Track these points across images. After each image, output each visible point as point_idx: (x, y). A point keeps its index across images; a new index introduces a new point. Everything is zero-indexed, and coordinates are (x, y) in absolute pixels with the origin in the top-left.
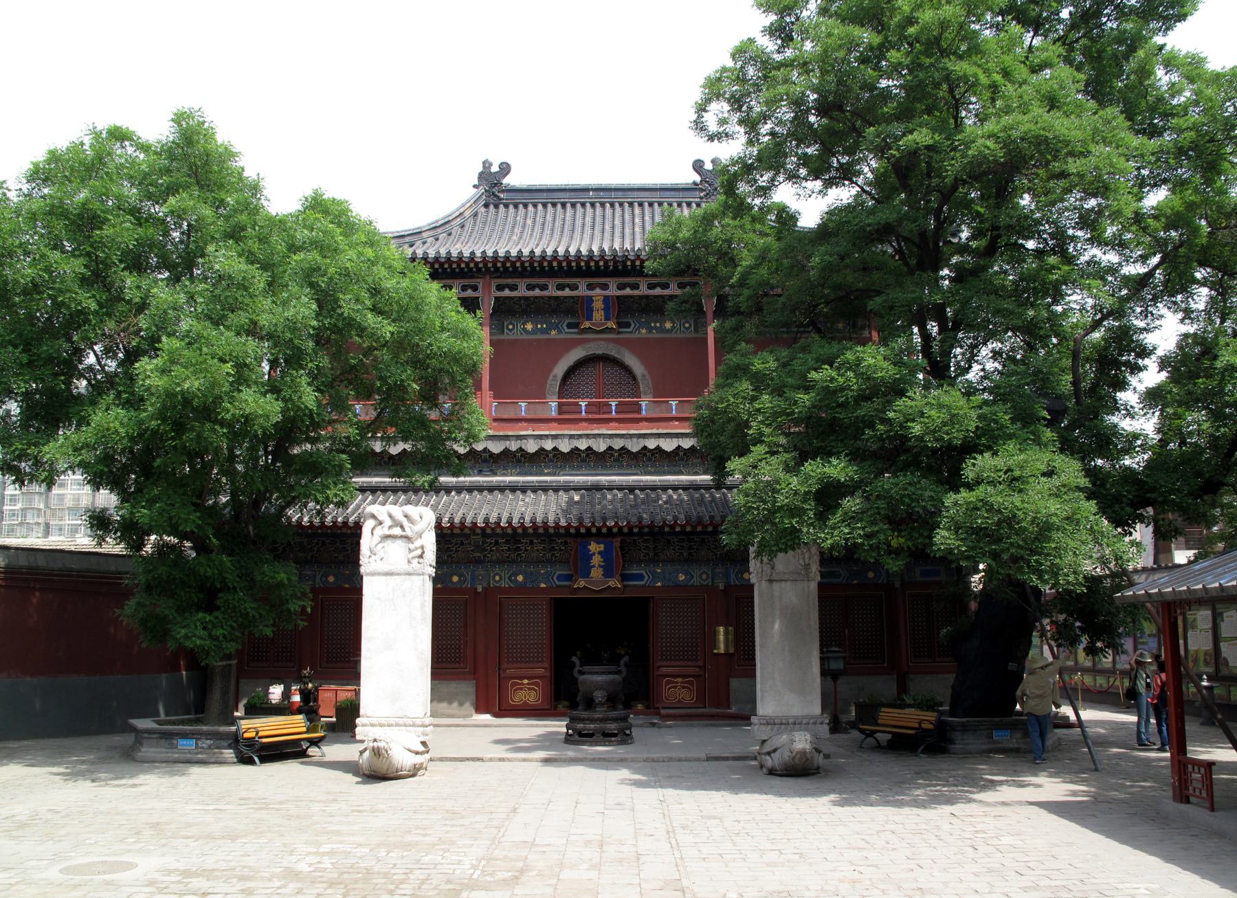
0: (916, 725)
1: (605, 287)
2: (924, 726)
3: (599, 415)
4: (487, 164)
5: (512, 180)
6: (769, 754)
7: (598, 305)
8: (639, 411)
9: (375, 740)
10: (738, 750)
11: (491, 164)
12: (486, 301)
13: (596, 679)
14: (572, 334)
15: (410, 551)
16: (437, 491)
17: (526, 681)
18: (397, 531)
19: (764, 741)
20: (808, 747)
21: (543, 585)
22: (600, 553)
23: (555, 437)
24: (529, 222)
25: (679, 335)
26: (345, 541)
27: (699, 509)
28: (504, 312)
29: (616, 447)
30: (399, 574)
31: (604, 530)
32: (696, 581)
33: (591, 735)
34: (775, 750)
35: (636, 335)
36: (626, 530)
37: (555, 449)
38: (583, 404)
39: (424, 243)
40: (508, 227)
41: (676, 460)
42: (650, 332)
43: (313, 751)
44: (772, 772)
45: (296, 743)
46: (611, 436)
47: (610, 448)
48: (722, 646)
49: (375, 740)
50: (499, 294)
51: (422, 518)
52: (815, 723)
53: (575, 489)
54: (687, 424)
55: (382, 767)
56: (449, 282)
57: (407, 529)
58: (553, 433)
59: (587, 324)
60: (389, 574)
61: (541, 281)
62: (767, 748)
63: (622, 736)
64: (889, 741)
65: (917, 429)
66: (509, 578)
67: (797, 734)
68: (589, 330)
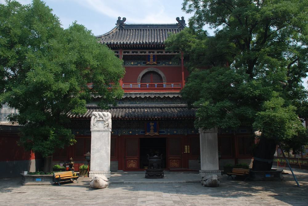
0: (244, 173)
1: (153, 52)
2: (246, 173)
3: (152, 88)
4: (119, 18)
5: (128, 22)
6: (205, 181)
7: (151, 57)
8: (163, 86)
9: (96, 178)
10: (195, 180)
11: (120, 18)
12: (121, 56)
13: (155, 159)
14: (144, 65)
15: (105, 124)
16: (116, 108)
17: (132, 161)
18: (101, 119)
19: (203, 177)
20: (217, 179)
21: (137, 134)
22: (153, 125)
23: (140, 94)
24: (131, 34)
25: (173, 66)
27: (180, 114)
28: (126, 58)
30: (101, 131)
31: (154, 119)
33: (153, 176)
34: (207, 180)
36: (160, 119)
37: (140, 97)
38: (148, 85)
39: (102, 40)
40: (126, 36)
41: (174, 99)
42: (166, 65)
43: (75, 181)
44: (206, 186)
45: (69, 179)
46: (155, 94)
47: (155, 97)
48: (186, 151)
49: (96, 178)
50: (124, 54)
51: (108, 115)
52: (217, 172)
53: (157, 108)
54: (179, 90)
55: (97, 185)
56: (117, 51)
57: (104, 119)
58: (140, 92)
59: (148, 63)
60: (99, 131)
61: (136, 51)
62: (204, 179)
63: (160, 176)
64: (235, 177)
65: (246, 92)
66: (128, 132)
67: (213, 175)
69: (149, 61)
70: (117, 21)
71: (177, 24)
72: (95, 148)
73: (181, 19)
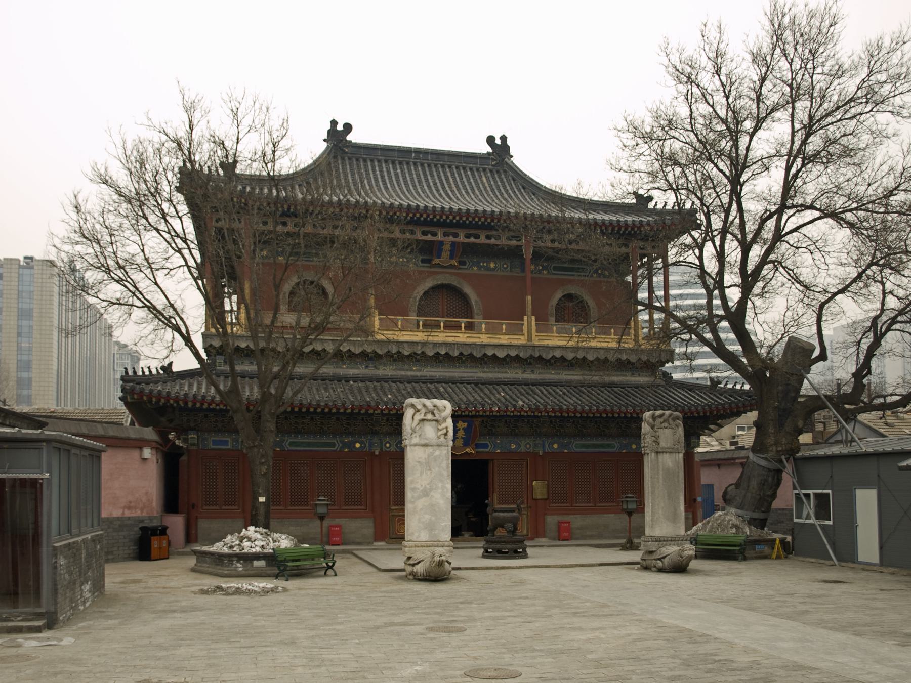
1: (456, 235)
6: (660, 559)
7: (447, 247)
11: (337, 123)
18: (429, 416)
26: (393, 422)
29: (465, 353)
32: (523, 449)
35: (470, 271)
59: (436, 261)
66: (396, 445)
68: (438, 265)
69: (439, 257)
70: (329, 131)
71: (488, 153)
72: (418, 486)
73: (498, 141)
